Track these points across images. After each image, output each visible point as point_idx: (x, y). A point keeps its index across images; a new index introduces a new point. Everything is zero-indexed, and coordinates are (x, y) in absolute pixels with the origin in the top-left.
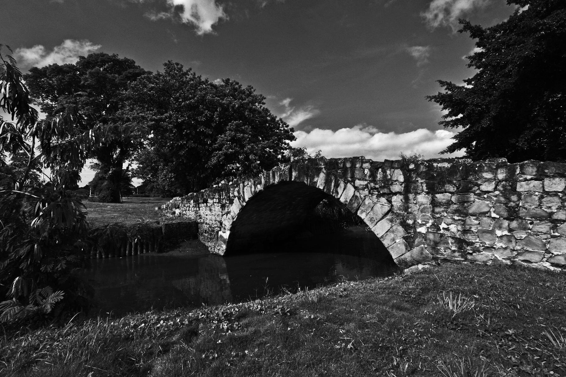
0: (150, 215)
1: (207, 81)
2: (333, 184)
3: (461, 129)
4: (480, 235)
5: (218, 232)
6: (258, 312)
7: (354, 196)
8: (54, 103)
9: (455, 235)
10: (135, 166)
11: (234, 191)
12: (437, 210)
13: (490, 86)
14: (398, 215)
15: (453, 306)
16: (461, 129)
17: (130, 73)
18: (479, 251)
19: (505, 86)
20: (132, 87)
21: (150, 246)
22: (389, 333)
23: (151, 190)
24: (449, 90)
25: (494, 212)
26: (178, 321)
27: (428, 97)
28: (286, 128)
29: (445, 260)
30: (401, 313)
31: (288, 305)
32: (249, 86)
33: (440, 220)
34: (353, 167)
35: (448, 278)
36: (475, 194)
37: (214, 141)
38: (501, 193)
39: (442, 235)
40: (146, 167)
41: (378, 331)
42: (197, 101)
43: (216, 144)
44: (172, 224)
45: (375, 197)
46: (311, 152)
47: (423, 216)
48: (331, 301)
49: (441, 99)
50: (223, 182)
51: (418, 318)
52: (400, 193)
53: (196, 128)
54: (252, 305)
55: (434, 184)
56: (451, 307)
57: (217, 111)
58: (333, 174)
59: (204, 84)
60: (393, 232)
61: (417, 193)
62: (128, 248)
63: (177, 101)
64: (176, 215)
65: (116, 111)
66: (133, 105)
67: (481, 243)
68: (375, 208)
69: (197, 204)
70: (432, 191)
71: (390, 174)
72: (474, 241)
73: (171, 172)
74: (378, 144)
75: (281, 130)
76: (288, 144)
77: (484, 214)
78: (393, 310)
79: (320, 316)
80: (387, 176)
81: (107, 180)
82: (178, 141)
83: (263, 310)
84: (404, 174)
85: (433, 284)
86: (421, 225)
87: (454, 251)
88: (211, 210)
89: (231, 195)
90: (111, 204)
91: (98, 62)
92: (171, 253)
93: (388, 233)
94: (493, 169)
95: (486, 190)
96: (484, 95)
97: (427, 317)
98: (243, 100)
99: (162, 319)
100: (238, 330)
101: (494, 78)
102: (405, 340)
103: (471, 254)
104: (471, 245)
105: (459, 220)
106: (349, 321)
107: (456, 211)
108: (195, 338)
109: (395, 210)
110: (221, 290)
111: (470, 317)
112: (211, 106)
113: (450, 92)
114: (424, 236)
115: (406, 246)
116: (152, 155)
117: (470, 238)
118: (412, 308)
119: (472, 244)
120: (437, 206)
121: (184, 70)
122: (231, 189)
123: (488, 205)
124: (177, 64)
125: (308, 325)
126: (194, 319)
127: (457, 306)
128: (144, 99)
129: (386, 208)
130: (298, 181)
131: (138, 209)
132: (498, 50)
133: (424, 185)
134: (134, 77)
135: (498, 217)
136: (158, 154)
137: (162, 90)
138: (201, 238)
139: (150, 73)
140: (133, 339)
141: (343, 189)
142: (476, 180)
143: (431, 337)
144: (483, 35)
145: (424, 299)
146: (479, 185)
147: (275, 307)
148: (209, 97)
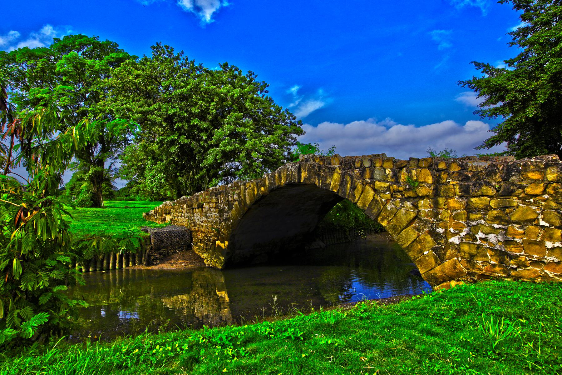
0: (137, 223)
1: (201, 66)
2: (349, 186)
3: (501, 119)
4: (526, 247)
5: (215, 242)
6: (266, 336)
7: (374, 201)
8: (24, 93)
9: (495, 247)
10: (118, 165)
11: (233, 194)
12: (473, 216)
13: (537, 68)
14: (426, 223)
15: (495, 332)
16: (501, 119)
17: (113, 58)
18: (525, 266)
19: (555, 68)
20: (115, 74)
21: (137, 258)
22: (420, 363)
23: (137, 192)
24: (486, 72)
25: (543, 219)
26: (177, 346)
27: (461, 82)
28: (293, 121)
29: (484, 277)
30: (433, 338)
31: (300, 328)
32: (249, 72)
33: (477, 228)
34: (373, 166)
35: (488, 298)
36: (519, 198)
37: (211, 136)
38: (552, 197)
39: (479, 247)
40: (131, 167)
41: (406, 359)
42: (191, 90)
43: (212, 140)
44: (163, 233)
45: (398, 201)
46: (323, 150)
47: (456, 223)
48: (350, 323)
49: (476, 86)
50: (220, 184)
51: (452, 345)
52: (428, 197)
53: (188, 121)
54: (259, 327)
55: (468, 186)
56: (492, 333)
57: (213, 101)
58: (349, 175)
59: (198, 70)
60: (420, 242)
61: (448, 197)
62: (111, 261)
63: (168, 90)
64: (166, 222)
65: (96, 102)
66: (117, 94)
67: (527, 256)
68: (399, 214)
69: (191, 208)
70: (466, 193)
71: (416, 175)
72: (518, 254)
73: (160, 172)
74: (395, 136)
75: (287, 123)
76: (295, 139)
77: (530, 221)
78: (423, 335)
79: (339, 342)
80: (413, 177)
81: (86, 181)
82: (168, 136)
83: (272, 334)
84: (433, 175)
85: (470, 305)
86: (454, 235)
87: (494, 266)
88: (206, 216)
89: (230, 199)
90: (91, 209)
91: (75, 45)
92: (161, 266)
93: (415, 244)
94: (540, 168)
95: (533, 193)
96: (530, 78)
97: (464, 344)
98: (243, 88)
99: (158, 344)
100: (245, 356)
101: (542, 58)
102: (438, 371)
103: (515, 269)
104: (515, 259)
105: (499, 228)
106: (371, 347)
107: (497, 218)
108: (196, 366)
109: (423, 216)
110: (219, 308)
111: (516, 345)
112: (206, 96)
113: (487, 76)
114: (458, 248)
115: (436, 259)
116: (138, 152)
117: (512, 250)
118: (445, 332)
119: (516, 257)
120: (472, 212)
121: (175, 54)
122: (230, 192)
123: (535, 211)
124: (167, 47)
125: (325, 351)
126: (195, 345)
127: (500, 332)
128: (129, 87)
129: (412, 214)
130: (308, 182)
131: (123, 215)
132: (547, 24)
133: (457, 188)
134: (117, 62)
135: (548, 225)
136: (145, 151)
137: (150, 77)
138: (195, 248)
139: (135, 58)
140: (126, 367)
141: (360, 192)
142: (520, 181)
143: (470, 368)
144: (530, 6)
145: (459, 323)
146: (523, 188)
147: (286, 330)
148: (204, 86)
